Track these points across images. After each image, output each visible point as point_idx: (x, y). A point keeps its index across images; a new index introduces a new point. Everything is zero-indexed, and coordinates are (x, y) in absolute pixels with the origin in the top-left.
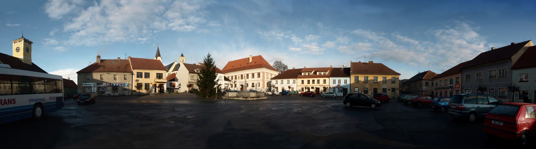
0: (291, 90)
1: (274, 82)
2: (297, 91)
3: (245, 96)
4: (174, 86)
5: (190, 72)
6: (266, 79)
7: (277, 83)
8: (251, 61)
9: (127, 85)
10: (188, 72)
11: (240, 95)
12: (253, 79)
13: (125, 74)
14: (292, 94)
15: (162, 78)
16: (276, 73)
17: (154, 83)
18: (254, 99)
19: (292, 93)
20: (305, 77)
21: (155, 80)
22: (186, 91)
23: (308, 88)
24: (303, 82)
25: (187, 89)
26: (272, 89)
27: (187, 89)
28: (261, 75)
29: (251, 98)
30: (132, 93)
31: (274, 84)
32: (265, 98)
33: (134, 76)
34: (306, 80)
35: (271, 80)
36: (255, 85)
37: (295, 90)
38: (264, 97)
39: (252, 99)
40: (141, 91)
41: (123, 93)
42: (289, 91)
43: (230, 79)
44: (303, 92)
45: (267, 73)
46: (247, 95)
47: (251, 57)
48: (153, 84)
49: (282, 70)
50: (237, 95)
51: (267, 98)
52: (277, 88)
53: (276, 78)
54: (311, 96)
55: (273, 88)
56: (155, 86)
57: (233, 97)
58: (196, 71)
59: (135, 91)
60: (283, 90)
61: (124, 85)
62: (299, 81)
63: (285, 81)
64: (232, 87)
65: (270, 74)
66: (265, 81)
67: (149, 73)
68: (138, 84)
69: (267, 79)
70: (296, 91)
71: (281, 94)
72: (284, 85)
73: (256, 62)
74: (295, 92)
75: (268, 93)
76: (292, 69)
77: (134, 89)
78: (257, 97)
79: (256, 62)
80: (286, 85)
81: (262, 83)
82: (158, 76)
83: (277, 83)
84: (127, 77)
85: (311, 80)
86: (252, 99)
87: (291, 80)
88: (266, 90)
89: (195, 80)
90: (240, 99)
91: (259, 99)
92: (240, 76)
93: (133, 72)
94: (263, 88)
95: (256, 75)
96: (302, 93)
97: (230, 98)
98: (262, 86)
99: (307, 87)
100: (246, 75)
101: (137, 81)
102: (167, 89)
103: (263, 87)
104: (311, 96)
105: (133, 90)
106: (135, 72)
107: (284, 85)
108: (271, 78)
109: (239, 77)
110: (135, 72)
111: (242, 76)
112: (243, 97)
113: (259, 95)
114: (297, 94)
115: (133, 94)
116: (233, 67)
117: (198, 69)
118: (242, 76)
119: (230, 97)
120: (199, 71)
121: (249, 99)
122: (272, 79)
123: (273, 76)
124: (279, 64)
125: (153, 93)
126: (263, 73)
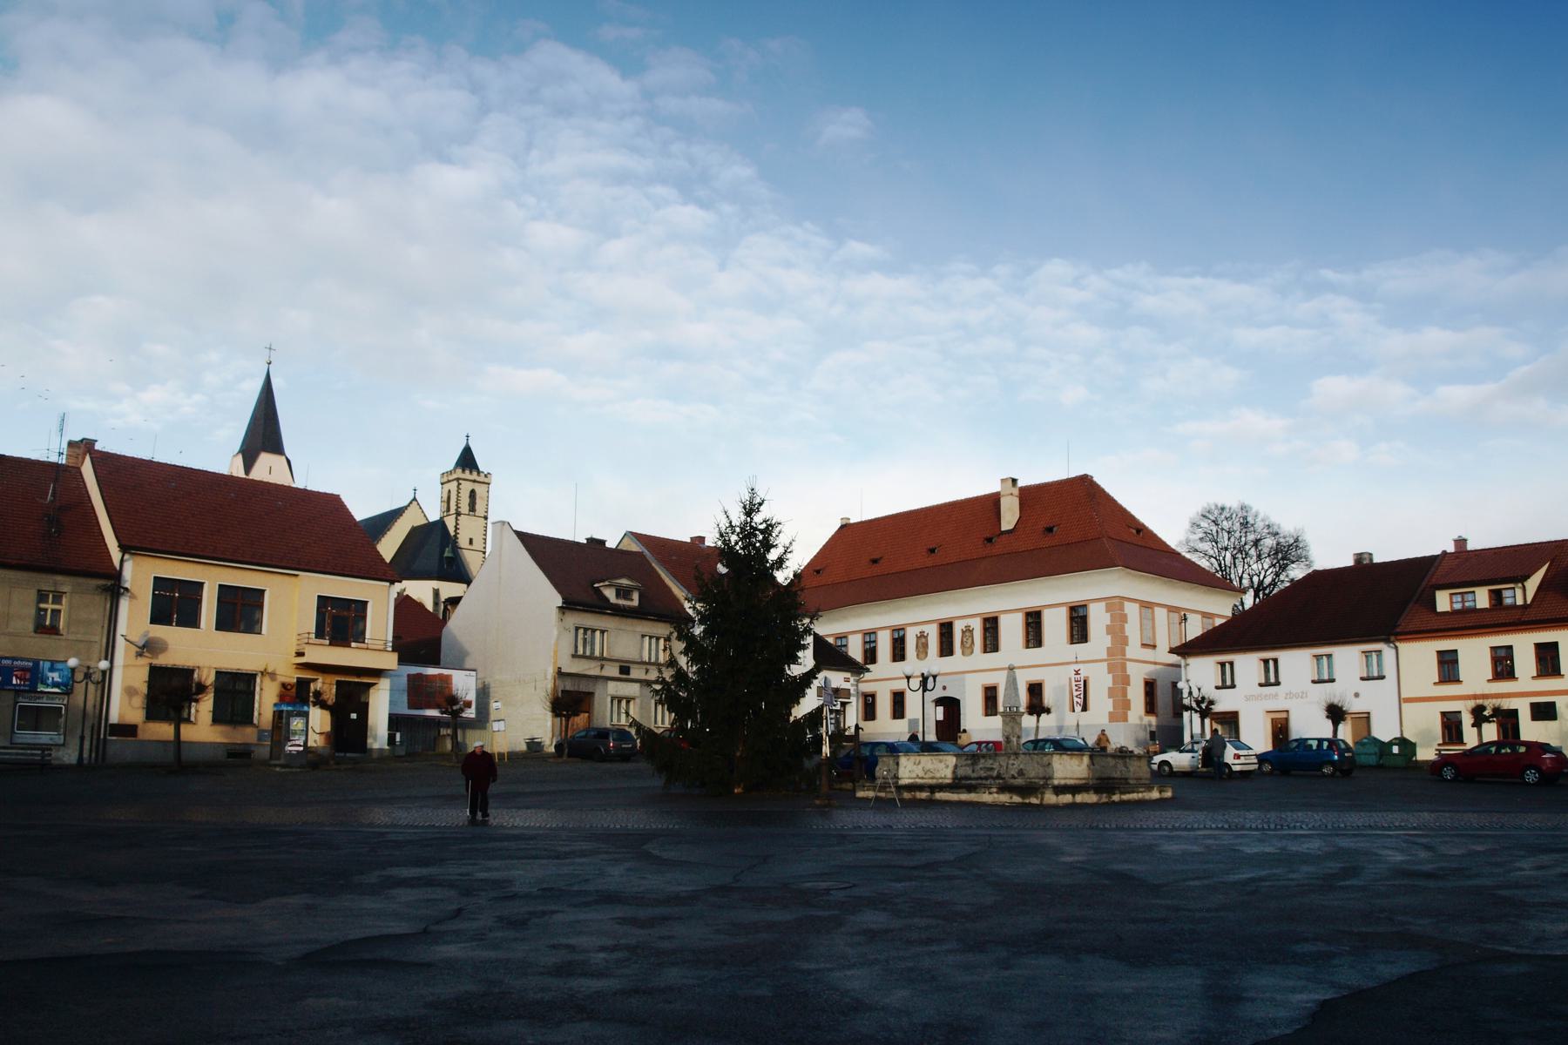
0: (1345, 733)
1: (1201, 674)
2: (1403, 742)
3: (1019, 781)
4: (451, 702)
5: (569, 606)
6: (1134, 650)
7: (1227, 684)
8: (1010, 516)
9: (55, 676)
10: (558, 600)
11: (983, 774)
12: (1035, 654)
13: (47, 582)
14: (1363, 767)
15: (361, 637)
16: (1221, 608)
17: (292, 676)
18: (1079, 798)
19: (1363, 760)
20: (1468, 623)
21: (307, 650)
22: (534, 745)
23: (1497, 711)
24: (1448, 667)
25: (542, 727)
26: (1193, 724)
27: (542, 727)
28: (1098, 619)
29: (1060, 790)
30: (100, 746)
31: (1209, 691)
32: (1155, 795)
33: (124, 604)
34: (1474, 653)
35: (1174, 658)
36: (1048, 698)
37: (1384, 731)
38: (1149, 788)
39: (1067, 798)
40: (188, 733)
41: (13, 745)
42: (1333, 742)
43: (855, 651)
44: (1455, 749)
45: (1147, 605)
46: (1033, 771)
47: (1016, 492)
48: (281, 679)
49: (1261, 569)
50: (961, 772)
51: (1173, 798)
52: (1230, 720)
53: (1217, 641)
54: (1531, 776)
55: (1196, 718)
56: (297, 695)
57: (933, 788)
58: (610, 594)
59: (127, 730)
60: (1280, 729)
61: (34, 675)
62: (1419, 656)
63: (1296, 663)
64: (869, 712)
65: (1172, 609)
66: (1129, 664)
67: (262, 592)
68: (156, 673)
69: (1148, 654)
70: (1391, 743)
71: (1267, 768)
72: (1289, 695)
73: (1050, 530)
74: (1384, 747)
75: (1168, 756)
76: (1349, 562)
77: (124, 706)
78: (1098, 790)
79: (1050, 530)
80: (1303, 695)
81: (1108, 680)
82: (328, 621)
83: (1227, 684)
84: (64, 607)
85: (1524, 645)
86: (1067, 798)
87: (1348, 658)
88: (1145, 735)
89: (602, 658)
90: (986, 798)
91: (1116, 798)
92: (933, 633)
93: (117, 576)
94: (1113, 717)
95: (1056, 625)
96: (1444, 761)
97: (906, 795)
98: (1108, 705)
99: (1490, 704)
100: (977, 626)
101: (148, 647)
102: (395, 721)
103: (1120, 712)
104: (1531, 776)
105: (114, 718)
106: (139, 574)
107: (1289, 695)
108: (1176, 644)
109: (922, 637)
110: (139, 574)
111: (946, 629)
112: (1003, 789)
113: (1117, 770)
114: (1400, 762)
115: (111, 750)
116: (875, 561)
117: (624, 582)
118: (946, 629)
119: (912, 788)
120: (636, 596)
121: (1050, 798)
122: (1187, 649)
123: (1195, 629)
124: (1237, 526)
125: (290, 754)
126: (1115, 605)
